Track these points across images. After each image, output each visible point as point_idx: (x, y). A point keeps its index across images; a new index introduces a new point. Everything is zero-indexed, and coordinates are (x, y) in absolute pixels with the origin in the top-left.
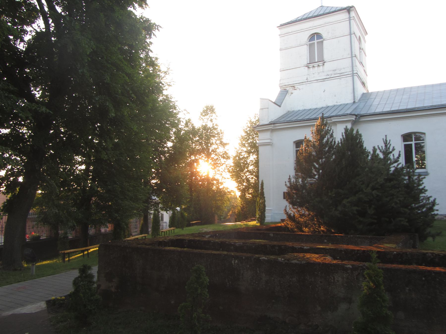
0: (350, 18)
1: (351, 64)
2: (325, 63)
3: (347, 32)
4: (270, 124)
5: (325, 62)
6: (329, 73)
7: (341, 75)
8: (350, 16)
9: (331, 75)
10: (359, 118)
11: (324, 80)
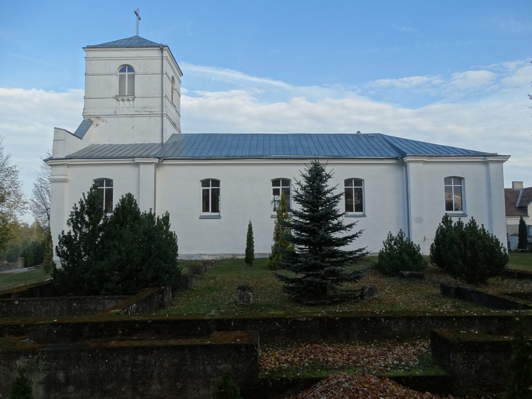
0: (162, 57)
1: (161, 103)
2: (135, 99)
3: (159, 71)
4: (66, 158)
5: (135, 97)
6: (139, 110)
7: (151, 114)
8: (162, 55)
9: (141, 111)
10: (162, 161)
11: (132, 116)
